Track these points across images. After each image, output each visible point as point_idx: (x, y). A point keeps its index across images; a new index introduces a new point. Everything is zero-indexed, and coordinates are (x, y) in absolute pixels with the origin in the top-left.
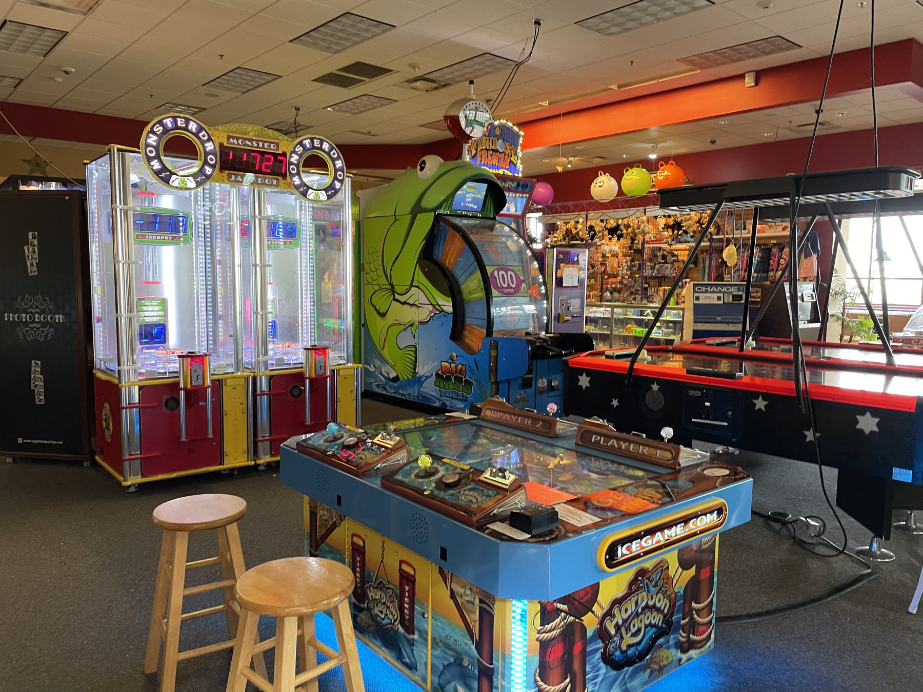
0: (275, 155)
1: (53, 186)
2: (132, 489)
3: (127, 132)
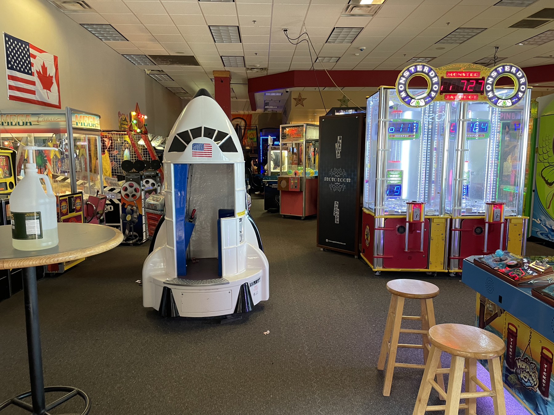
0: (477, 80)
1: (351, 112)
2: (377, 274)
3: (388, 78)
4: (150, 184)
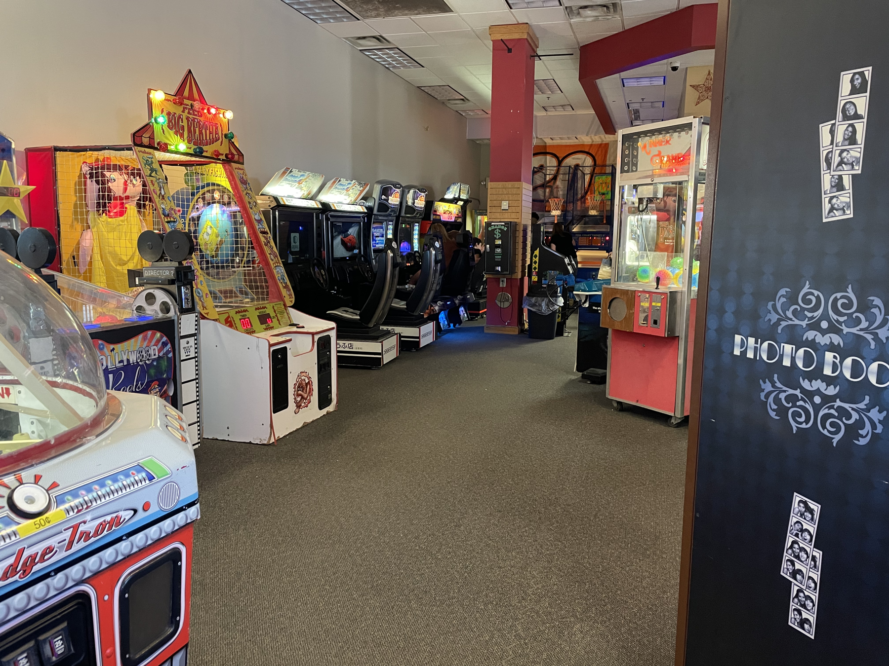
4: (157, 306)
